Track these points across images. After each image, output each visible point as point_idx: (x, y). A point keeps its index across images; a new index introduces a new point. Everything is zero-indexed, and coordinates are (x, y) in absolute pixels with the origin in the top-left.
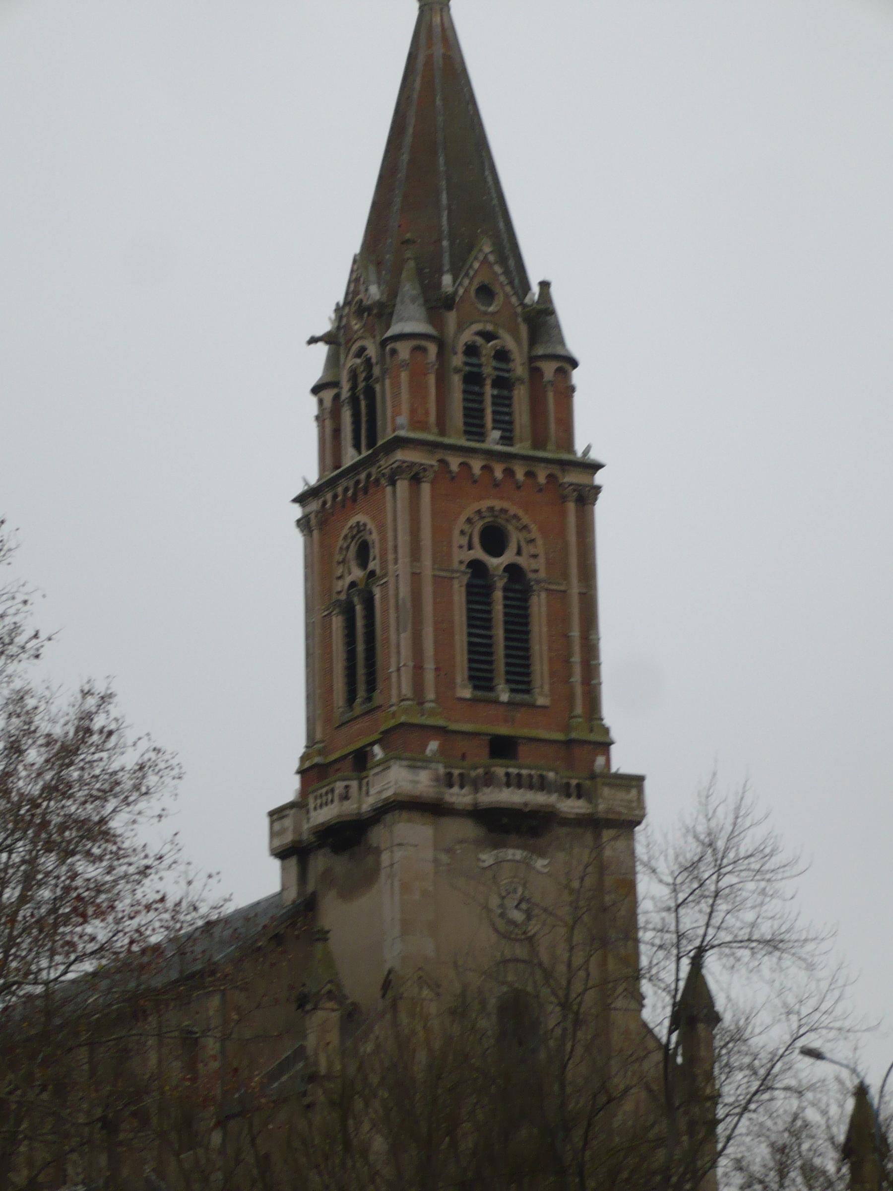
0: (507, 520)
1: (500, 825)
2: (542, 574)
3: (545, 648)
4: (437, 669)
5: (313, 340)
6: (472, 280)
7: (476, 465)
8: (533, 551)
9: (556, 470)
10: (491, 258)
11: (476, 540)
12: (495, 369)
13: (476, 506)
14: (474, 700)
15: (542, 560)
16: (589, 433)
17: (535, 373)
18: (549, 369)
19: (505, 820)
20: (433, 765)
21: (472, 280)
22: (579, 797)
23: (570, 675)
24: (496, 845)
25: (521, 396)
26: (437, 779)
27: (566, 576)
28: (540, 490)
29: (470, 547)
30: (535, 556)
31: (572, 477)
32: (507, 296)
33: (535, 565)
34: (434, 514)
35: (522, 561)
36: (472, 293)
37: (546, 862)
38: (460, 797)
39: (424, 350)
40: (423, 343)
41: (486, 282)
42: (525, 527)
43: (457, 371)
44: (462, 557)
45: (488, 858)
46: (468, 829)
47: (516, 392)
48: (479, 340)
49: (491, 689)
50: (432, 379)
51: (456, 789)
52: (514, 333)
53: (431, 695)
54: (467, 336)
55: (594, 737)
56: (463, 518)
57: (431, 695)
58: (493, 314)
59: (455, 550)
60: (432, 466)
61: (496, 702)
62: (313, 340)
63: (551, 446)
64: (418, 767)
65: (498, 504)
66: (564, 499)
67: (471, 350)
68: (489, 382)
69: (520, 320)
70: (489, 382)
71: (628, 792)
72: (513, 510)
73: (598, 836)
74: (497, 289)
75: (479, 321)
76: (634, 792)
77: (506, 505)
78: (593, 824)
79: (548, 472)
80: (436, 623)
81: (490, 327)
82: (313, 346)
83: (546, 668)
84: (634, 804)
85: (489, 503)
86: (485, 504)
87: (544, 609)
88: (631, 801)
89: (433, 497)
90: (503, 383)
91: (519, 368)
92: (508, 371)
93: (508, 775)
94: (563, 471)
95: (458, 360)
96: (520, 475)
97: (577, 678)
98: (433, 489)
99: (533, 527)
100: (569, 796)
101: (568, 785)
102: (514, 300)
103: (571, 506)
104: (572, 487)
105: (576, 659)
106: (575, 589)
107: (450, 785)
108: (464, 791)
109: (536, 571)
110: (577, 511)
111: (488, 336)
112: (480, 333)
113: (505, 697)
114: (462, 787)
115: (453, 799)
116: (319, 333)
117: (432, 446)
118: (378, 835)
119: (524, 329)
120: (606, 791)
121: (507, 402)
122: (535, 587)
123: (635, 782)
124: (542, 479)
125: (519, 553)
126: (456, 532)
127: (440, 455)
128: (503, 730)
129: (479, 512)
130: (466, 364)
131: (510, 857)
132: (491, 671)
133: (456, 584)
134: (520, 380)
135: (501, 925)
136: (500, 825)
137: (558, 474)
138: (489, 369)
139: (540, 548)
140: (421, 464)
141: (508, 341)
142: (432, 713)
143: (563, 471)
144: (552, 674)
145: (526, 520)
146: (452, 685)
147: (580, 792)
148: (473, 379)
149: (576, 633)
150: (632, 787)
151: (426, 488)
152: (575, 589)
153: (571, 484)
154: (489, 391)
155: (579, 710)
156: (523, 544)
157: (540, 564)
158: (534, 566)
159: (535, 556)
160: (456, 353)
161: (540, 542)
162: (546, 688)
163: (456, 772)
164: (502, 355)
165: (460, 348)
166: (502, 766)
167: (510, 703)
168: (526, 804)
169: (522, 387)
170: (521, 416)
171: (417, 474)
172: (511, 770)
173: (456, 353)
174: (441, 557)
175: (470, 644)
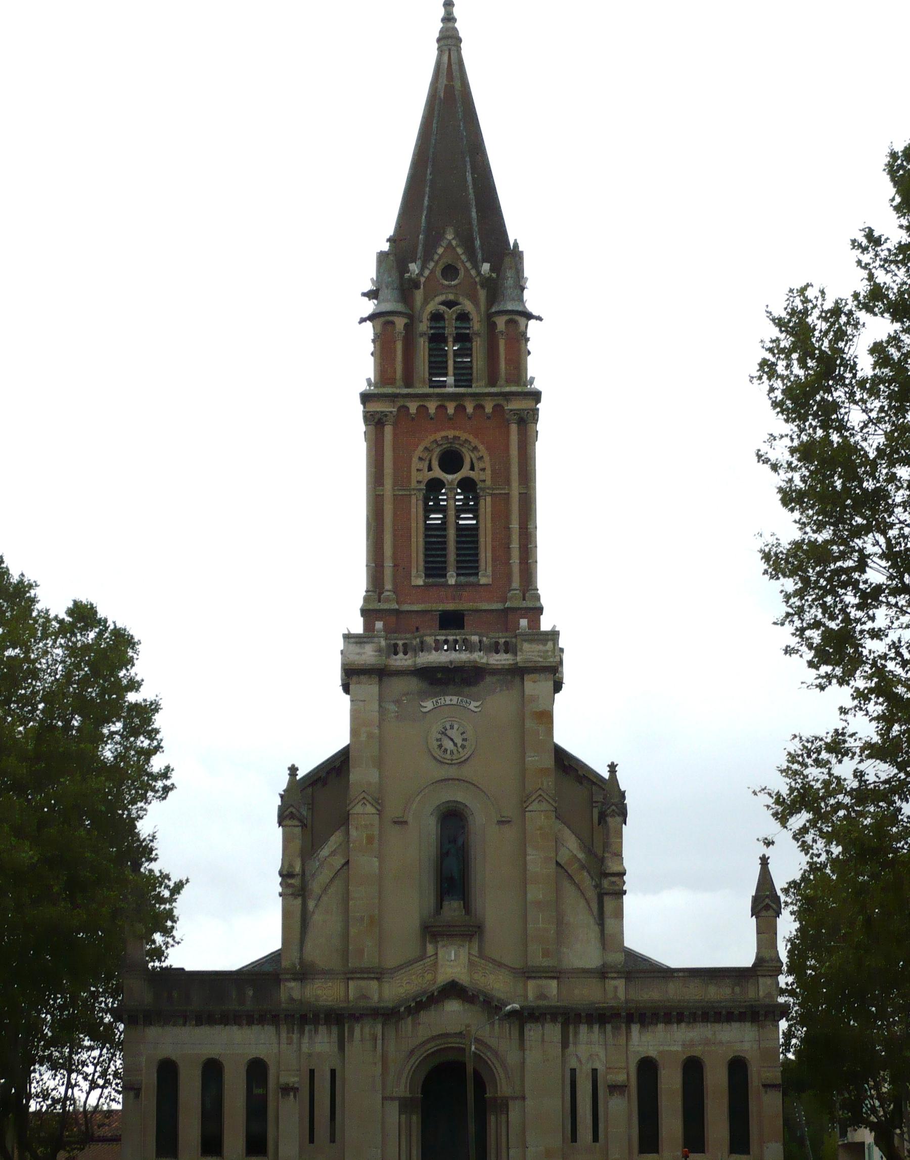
0: (461, 445)
1: (438, 679)
2: (488, 483)
3: (489, 539)
4: (395, 566)
5: (362, 320)
6: (437, 262)
7: (432, 406)
8: (482, 465)
9: (500, 400)
10: (454, 243)
11: (435, 464)
12: (456, 328)
13: (432, 438)
14: (426, 585)
15: (488, 472)
16: (539, 368)
17: (492, 326)
18: (501, 322)
19: (439, 676)
20: (376, 640)
21: (437, 262)
22: (506, 652)
23: (509, 558)
24: (435, 695)
25: (478, 345)
26: (379, 650)
27: (508, 482)
28: (489, 418)
29: (430, 469)
30: (483, 470)
31: (515, 405)
32: (467, 270)
33: (483, 476)
34: (395, 449)
35: (472, 474)
36: (438, 273)
37: (478, 704)
38: (401, 661)
39: (393, 323)
40: (391, 318)
41: (450, 263)
42: (475, 449)
43: (422, 335)
44: (420, 478)
45: (429, 705)
46: (413, 684)
47: (474, 343)
48: (443, 308)
49: (445, 576)
50: (399, 346)
51: (401, 655)
52: (474, 300)
53: (388, 586)
54: (431, 307)
55: (530, 604)
56: (421, 448)
57: (388, 586)
58: (455, 286)
59: (414, 472)
60: (391, 412)
61: (445, 585)
62: (362, 320)
63: (502, 381)
64: (365, 642)
65: (451, 434)
66: (507, 424)
67: (436, 317)
68: (450, 339)
69: (478, 287)
70: (450, 339)
71: (545, 645)
72: (464, 436)
73: (523, 679)
74: (460, 266)
75: (442, 294)
76: (550, 644)
77: (457, 433)
78: (518, 672)
79: (494, 403)
80: (395, 531)
81: (451, 297)
82: (364, 324)
83: (489, 555)
84: (550, 653)
85: (443, 434)
86: (439, 436)
87: (489, 510)
88: (547, 651)
89: (395, 435)
90: (463, 338)
91: (477, 325)
92: (469, 328)
93: (436, 641)
94: (507, 401)
95: (424, 326)
96: (470, 409)
97: (515, 559)
98: (394, 429)
99: (481, 447)
100: (497, 652)
101: (497, 643)
102: (473, 272)
103: (514, 428)
104: (516, 412)
105: (515, 545)
106: (515, 490)
107: (396, 653)
108: (407, 657)
109: (484, 481)
110: (519, 430)
111: (450, 304)
112: (443, 303)
113: (452, 581)
114: (405, 653)
115: (398, 663)
116: (366, 315)
117: (393, 397)
118: (488, 679)
119: (482, 294)
120: (526, 646)
121: (469, 352)
122: (481, 494)
123: (554, 635)
124: (489, 409)
125: (472, 468)
126: (415, 460)
127: (401, 402)
128: (451, 606)
129: (435, 441)
130: (431, 328)
131: (448, 702)
132: (445, 562)
133: (414, 500)
134: (478, 334)
135: (438, 753)
136: (438, 679)
137: (504, 403)
138: (450, 331)
139: (487, 463)
140: (382, 412)
141: (468, 306)
142: (388, 600)
143: (507, 401)
144: (494, 560)
145: (475, 442)
146: (409, 576)
147: (508, 648)
148: (437, 339)
149: (515, 526)
150: (547, 640)
151: (388, 430)
152: (515, 490)
153: (511, 410)
154: (452, 347)
155: (516, 584)
156: (475, 461)
157: (487, 475)
158: (483, 478)
159: (483, 470)
160: (421, 322)
161: (487, 458)
162: (489, 570)
163: (400, 643)
164: (463, 317)
165: (426, 316)
166: (430, 635)
167: (457, 585)
168: (451, 662)
169: (478, 339)
170: (479, 361)
171: (380, 419)
172: (438, 638)
173: (421, 322)
174: (402, 479)
175: (426, 543)
